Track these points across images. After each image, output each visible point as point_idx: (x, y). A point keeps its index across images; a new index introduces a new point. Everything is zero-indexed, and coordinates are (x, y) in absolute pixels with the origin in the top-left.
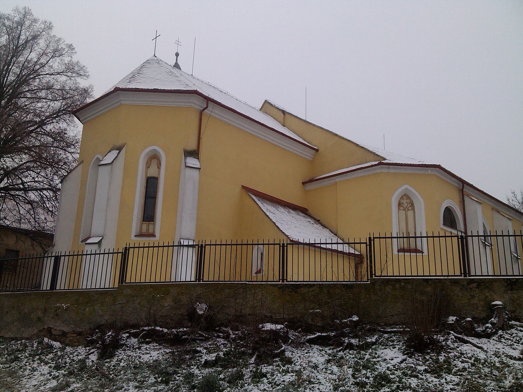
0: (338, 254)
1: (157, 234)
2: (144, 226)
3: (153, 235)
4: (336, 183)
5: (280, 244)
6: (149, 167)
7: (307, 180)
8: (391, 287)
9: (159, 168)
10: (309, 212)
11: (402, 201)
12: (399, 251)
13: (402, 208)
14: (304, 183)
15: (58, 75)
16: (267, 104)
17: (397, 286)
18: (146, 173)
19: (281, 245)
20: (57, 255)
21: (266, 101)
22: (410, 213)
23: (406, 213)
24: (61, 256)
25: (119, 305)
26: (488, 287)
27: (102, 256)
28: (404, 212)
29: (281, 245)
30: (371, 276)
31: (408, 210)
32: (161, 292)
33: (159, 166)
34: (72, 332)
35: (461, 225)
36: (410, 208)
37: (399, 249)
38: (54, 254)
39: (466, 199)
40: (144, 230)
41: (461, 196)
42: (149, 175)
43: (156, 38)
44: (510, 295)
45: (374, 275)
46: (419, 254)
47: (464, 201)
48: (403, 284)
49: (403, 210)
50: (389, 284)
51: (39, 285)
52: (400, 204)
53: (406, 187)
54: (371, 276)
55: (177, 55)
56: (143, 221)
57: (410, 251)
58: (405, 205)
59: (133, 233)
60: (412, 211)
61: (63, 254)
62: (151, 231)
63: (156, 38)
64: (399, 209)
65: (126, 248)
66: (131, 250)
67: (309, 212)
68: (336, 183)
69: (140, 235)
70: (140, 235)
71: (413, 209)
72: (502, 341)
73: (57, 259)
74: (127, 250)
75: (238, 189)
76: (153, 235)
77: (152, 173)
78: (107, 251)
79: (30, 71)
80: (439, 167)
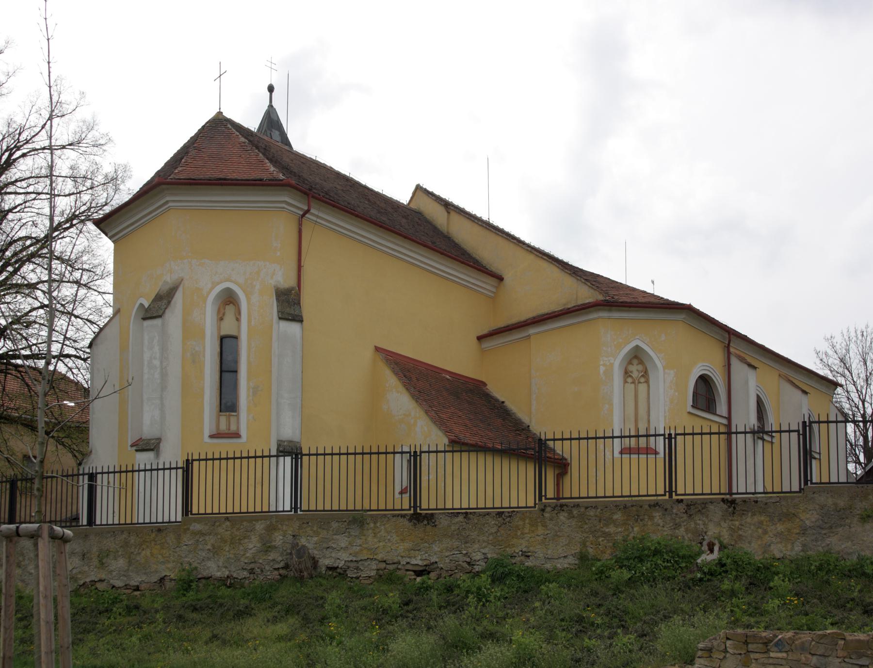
0: (561, 453)
1: (243, 432)
2: (223, 420)
3: (237, 435)
4: (529, 336)
5: (410, 453)
6: (221, 319)
7: (485, 331)
8: (566, 515)
9: (238, 320)
10: (487, 387)
11: (631, 368)
12: (621, 453)
13: (629, 380)
14: (480, 338)
15: (64, 150)
16: (419, 193)
17: (575, 512)
18: (219, 329)
19: (412, 454)
20: (91, 472)
21: (418, 188)
22: (642, 388)
23: (635, 388)
24: (97, 473)
25: (185, 547)
26: (699, 511)
27: (161, 472)
28: (633, 386)
29: (412, 454)
30: (540, 499)
31: (640, 382)
32: (242, 527)
33: (238, 317)
34: (125, 587)
35: (722, 409)
36: (642, 380)
37: (623, 447)
38: (86, 471)
39: (734, 362)
40: (223, 427)
41: (726, 355)
42: (223, 333)
43: (220, 75)
44: (730, 523)
45: (543, 498)
46: (651, 457)
47: (729, 365)
48: (583, 510)
49: (631, 383)
50: (563, 510)
51: (77, 514)
52: (627, 373)
53: (635, 345)
54: (540, 499)
55: (271, 89)
56: (221, 411)
57: (638, 451)
58: (635, 375)
59: (207, 433)
60: (645, 385)
61: (99, 470)
62: (233, 428)
63: (220, 75)
64: (625, 382)
65: (188, 460)
66: (196, 464)
67: (487, 387)
68: (529, 336)
69: (217, 435)
70: (217, 435)
71: (647, 382)
72: (210, 600)
73: (92, 477)
74: (189, 463)
75: (368, 353)
76: (237, 435)
77: (228, 328)
78: (167, 466)
79: (14, 142)
80: (688, 309)
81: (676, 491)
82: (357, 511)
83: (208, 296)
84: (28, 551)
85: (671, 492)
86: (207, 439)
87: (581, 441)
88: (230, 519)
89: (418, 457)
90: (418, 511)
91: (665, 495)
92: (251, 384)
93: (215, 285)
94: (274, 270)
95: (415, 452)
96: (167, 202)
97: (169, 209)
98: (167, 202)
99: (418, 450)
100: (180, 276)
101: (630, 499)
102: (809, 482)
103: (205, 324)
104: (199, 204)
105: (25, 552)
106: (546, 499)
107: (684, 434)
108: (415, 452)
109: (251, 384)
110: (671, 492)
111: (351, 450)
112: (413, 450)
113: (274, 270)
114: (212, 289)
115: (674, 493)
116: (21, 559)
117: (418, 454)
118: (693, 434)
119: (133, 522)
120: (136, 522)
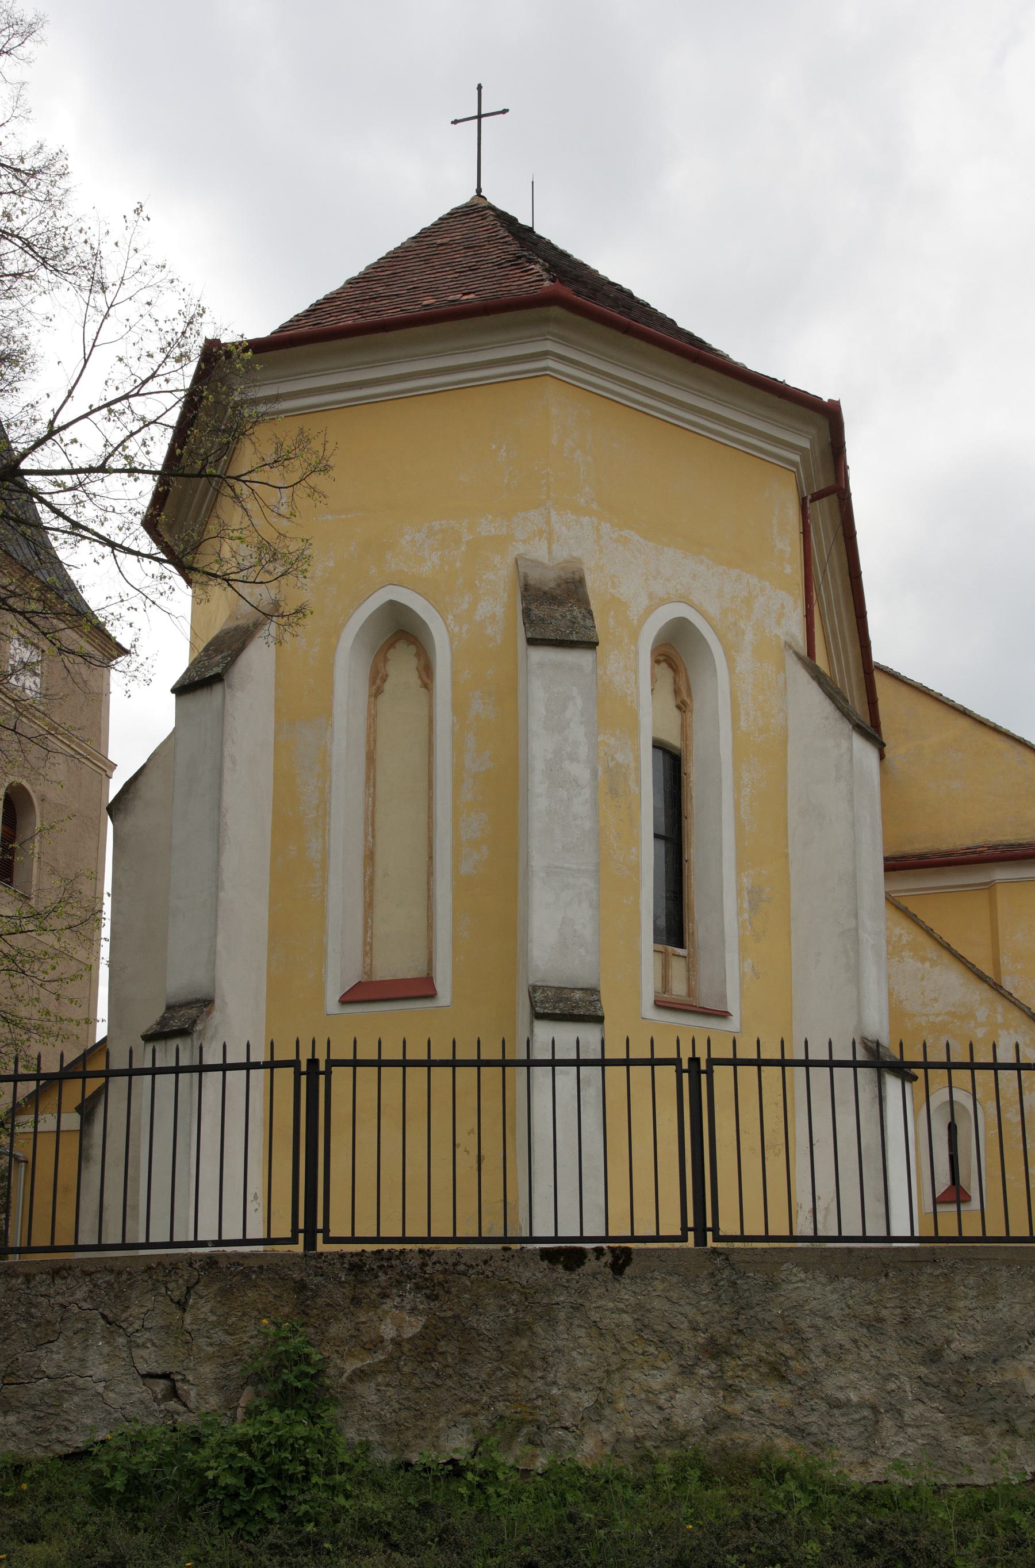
3: (724, 1015)
19: (304, 1068)
27: (213, 1079)
29: (304, 1068)
81: (326, 1230)
82: (204, 1244)
83: (641, 624)
84: (819, 1321)
85: (311, 1232)
86: (649, 1011)
87: (434, 1070)
88: (734, 1258)
89: (322, 1078)
90: (321, 1247)
91: (293, 1240)
92: (745, 880)
93: (656, 602)
94: (783, 606)
95: (313, 1062)
96: (544, 355)
97: (543, 374)
98: (544, 355)
99: (321, 1056)
100: (575, 554)
101: (269, 1248)
102: (709, 1234)
103: (638, 695)
104: (616, 388)
105: (803, 1324)
106: (717, 1238)
107: (355, 1063)
108: (313, 1062)
109: (745, 880)
110: (311, 1232)
111: (467, 1053)
112: (305, 1056)
113: (783, 606)
114: (649, 611)
115: (320, 1237)
116: (787, 1349)
117: (322, 1067)
118: (404, 1064)
119: (129, 1240)
120: (142, 1240)
